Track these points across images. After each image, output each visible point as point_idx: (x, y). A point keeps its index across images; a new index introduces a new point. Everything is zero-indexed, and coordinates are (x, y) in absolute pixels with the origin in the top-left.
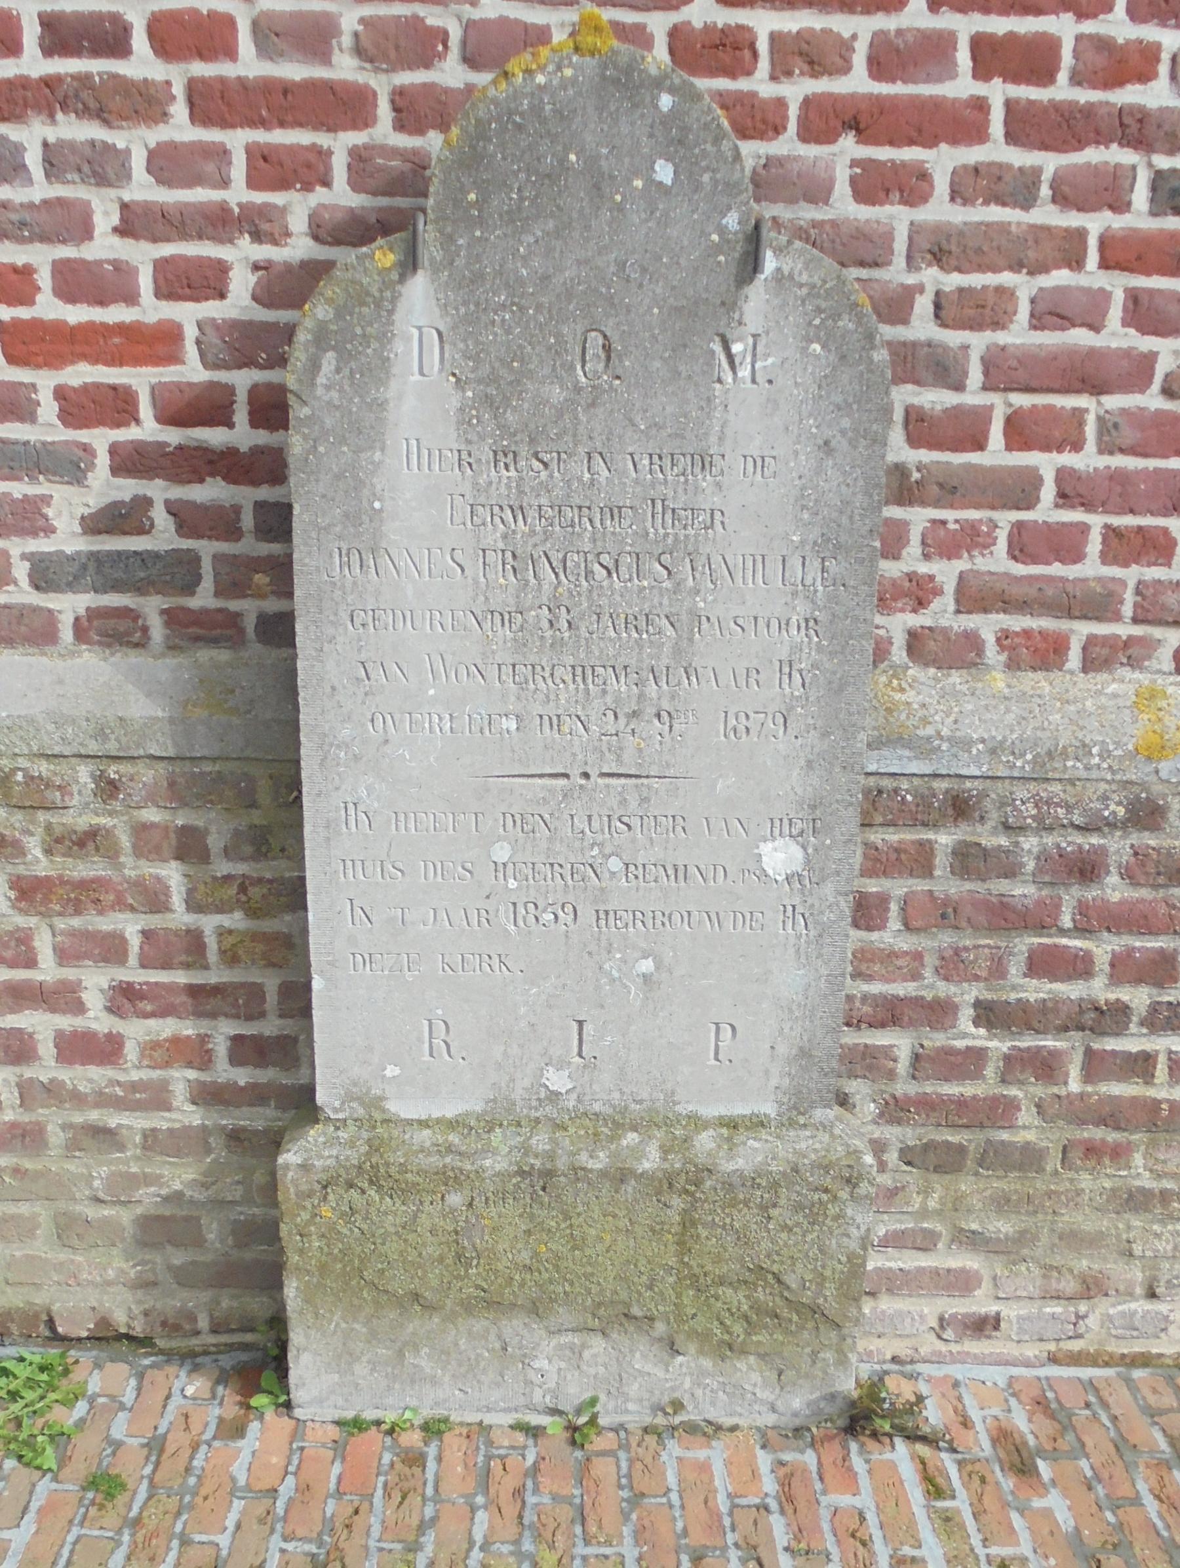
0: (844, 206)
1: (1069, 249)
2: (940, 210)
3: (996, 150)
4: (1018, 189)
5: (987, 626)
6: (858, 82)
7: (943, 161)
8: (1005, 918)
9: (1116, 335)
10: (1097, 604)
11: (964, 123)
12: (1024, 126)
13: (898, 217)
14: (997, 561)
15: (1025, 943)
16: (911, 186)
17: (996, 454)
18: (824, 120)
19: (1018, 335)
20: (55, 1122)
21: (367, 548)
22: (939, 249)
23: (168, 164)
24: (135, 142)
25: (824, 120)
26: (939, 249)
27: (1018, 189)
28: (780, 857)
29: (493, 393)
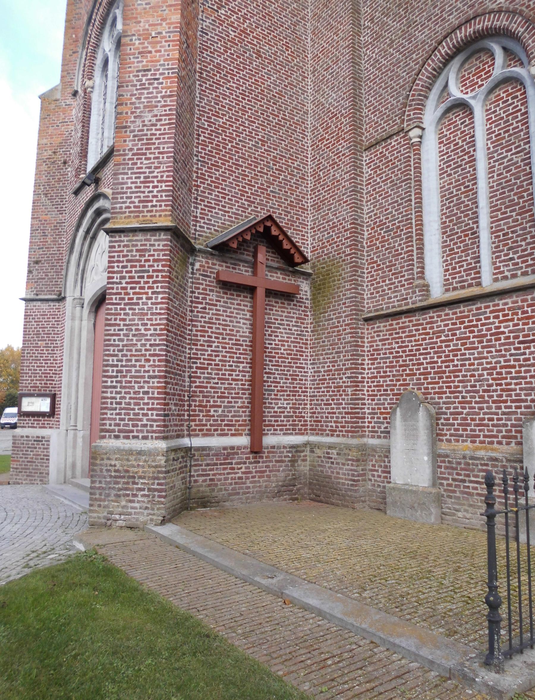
0: (437, 400)
1: (455, 403)
2: (444, 400)
3: (448, 395)
4: (450, 398)
5: (452, 438)
6: (437, 390)
7: (444, 396)
8: (453, 468)
9: (460, 410)
10: (462, 436)
11: (445, 393)
12: (451, 392)
13: (441, 401)
14: (452, 432)
15: (455, 472)
16: (442, 398)
17: (451, 421)
18: (435, 393)
19: (452, 410)
20: (199, 198)
21: (395, 429)
22: (444, 403)
23: (391, 399)
24: (388, 398)
25: (435, 393)
26: (444, 403)
27: (450, 398)
28: (426, 458)
29: (405, 418)
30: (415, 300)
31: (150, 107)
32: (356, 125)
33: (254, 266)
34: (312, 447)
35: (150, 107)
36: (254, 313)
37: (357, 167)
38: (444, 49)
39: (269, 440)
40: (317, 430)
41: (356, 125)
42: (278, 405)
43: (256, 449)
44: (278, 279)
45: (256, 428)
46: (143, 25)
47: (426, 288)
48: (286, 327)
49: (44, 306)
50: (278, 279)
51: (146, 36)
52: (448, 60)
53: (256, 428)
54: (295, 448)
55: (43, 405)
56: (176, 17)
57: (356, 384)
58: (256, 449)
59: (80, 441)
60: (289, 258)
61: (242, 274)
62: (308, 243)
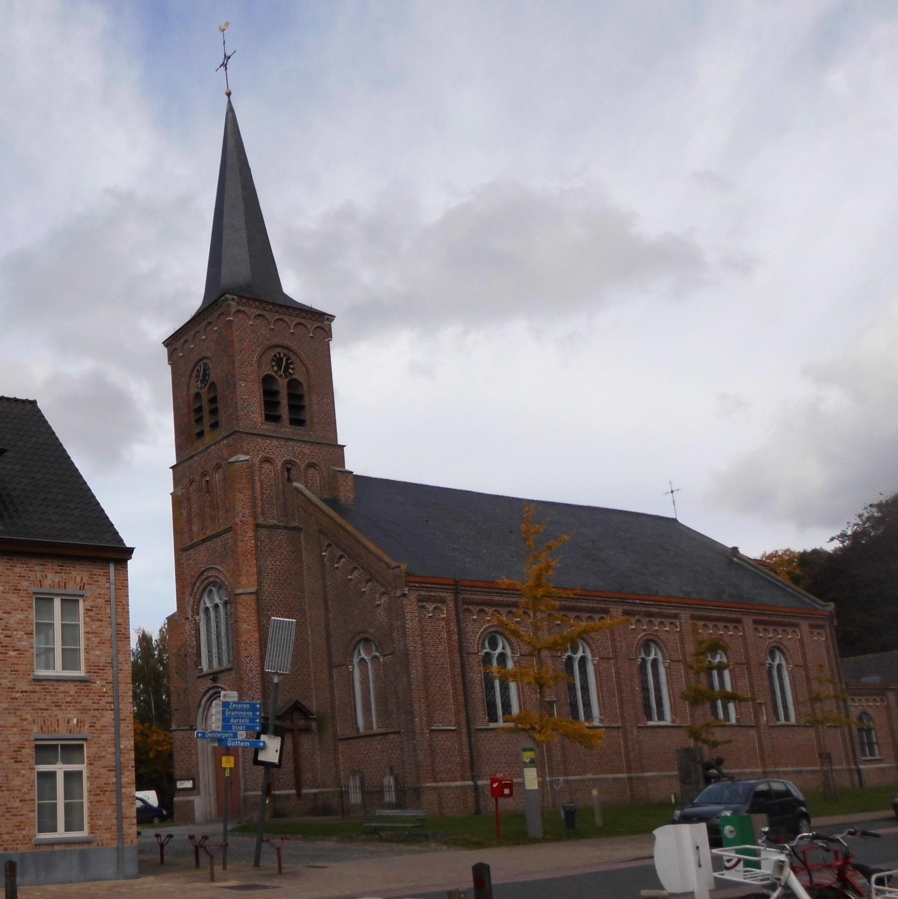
30: (354, 734)
31: (251, 671)
32: (330, 655)
33: (292, 720)
34: (322, 793)
35: (251, 671)
36: (293, 739)
37: (331, 675)
38: (354, 642)
39: (304, 791)
40: (324, 786)
41: (330, 655)
42: (307, 776)
43: (299, 795)
44: (302, 723)
45: (298, 786)
46: (244, 639)
47: (358, 729)
48: (307, 743)
49: (183, 733)
50: (302, 723)
51: (246, 643)
52: (359, 642)
53: (298, 786)
54: (315, 795)
55: (189, 784)
56: (257, 636)
57: (337, 766)
58: (299, 795)
59: (212, 800)
60: (305, 713)
61: (287, 724)
62: (313, 705)
